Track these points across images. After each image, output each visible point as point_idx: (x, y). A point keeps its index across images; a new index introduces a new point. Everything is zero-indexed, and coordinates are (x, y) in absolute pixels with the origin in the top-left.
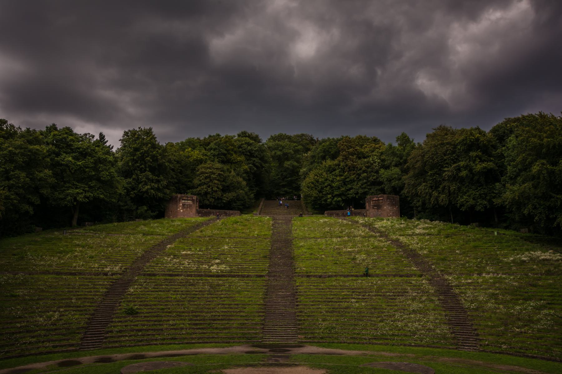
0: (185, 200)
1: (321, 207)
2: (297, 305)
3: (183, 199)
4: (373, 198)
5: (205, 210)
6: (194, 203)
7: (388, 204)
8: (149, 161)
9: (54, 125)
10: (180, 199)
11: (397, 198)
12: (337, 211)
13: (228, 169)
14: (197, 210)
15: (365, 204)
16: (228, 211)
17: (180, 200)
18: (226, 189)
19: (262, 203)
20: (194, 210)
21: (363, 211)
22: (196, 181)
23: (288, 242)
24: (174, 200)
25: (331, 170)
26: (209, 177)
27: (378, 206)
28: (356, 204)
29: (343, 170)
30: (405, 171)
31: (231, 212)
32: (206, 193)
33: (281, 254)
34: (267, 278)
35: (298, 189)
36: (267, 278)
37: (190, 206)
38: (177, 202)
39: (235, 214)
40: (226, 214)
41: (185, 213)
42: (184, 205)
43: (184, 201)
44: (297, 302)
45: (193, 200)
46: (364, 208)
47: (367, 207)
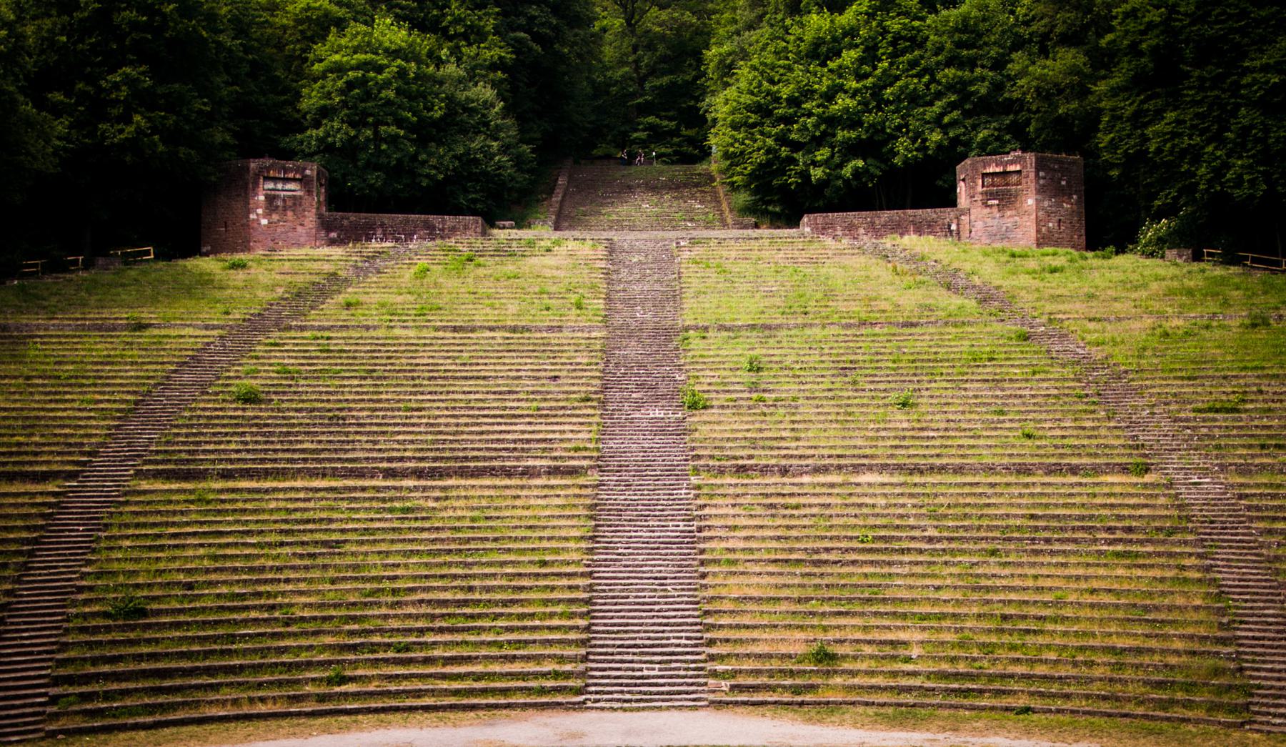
0: (275, 179)
1: (780, 198)
2: (704, 576)
3: (267, 179)
5: (353, 217)
6: (309, 192)
8: (134, 25)
9: (1039, 245)
10: (257, 176)
12: (853, 217)
13: (430, 54)
14: (320, 216)
15: (953, 188)
16: (435, 220)
17: (256, 184)
18: (427, 132)
19: (562, 181)
20: (311, 218)
21: (947, 214)
22: (311, 99)
23: (668, 337)
24: (241, 186)
25: (822, 51)
26: (363, 82)
28: (915, 188)
29: (871, 55)
30: (1103, 61)
31: (450, 220)
32: (351, 149)
33: (640, 386)
34: (594, 477)
35: (700, 121)
36: (594, 477)
37: (295, 204)
38: (246, 188)
39: (466, 228)
40: (432, 232)
42: (271, 199)
43: (271, 185)
44: (702, 563)
45: (304, 181)
46: (951, 202)
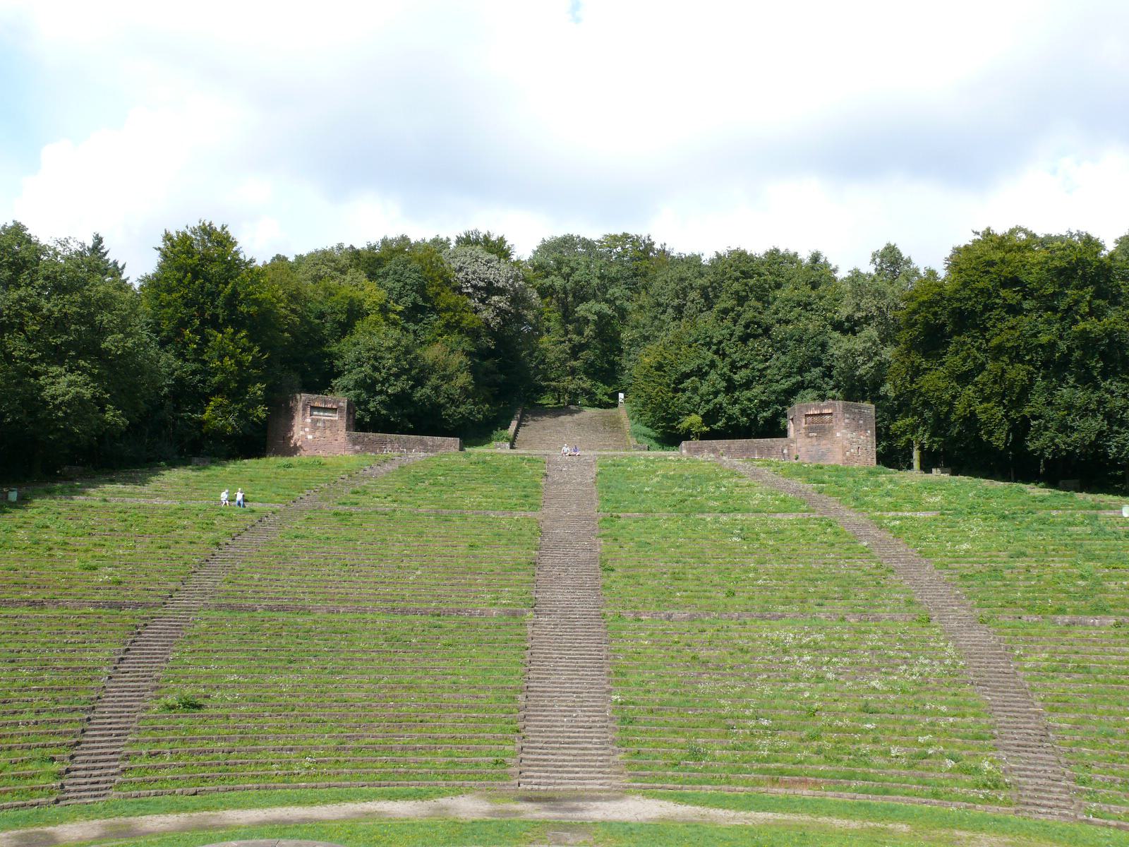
4: (808, 408)
7: (846, 427)
11: (869, 408)
27: (819, 428)
31: (438, 440)
41: (318, 429)
47: (791, 433)
